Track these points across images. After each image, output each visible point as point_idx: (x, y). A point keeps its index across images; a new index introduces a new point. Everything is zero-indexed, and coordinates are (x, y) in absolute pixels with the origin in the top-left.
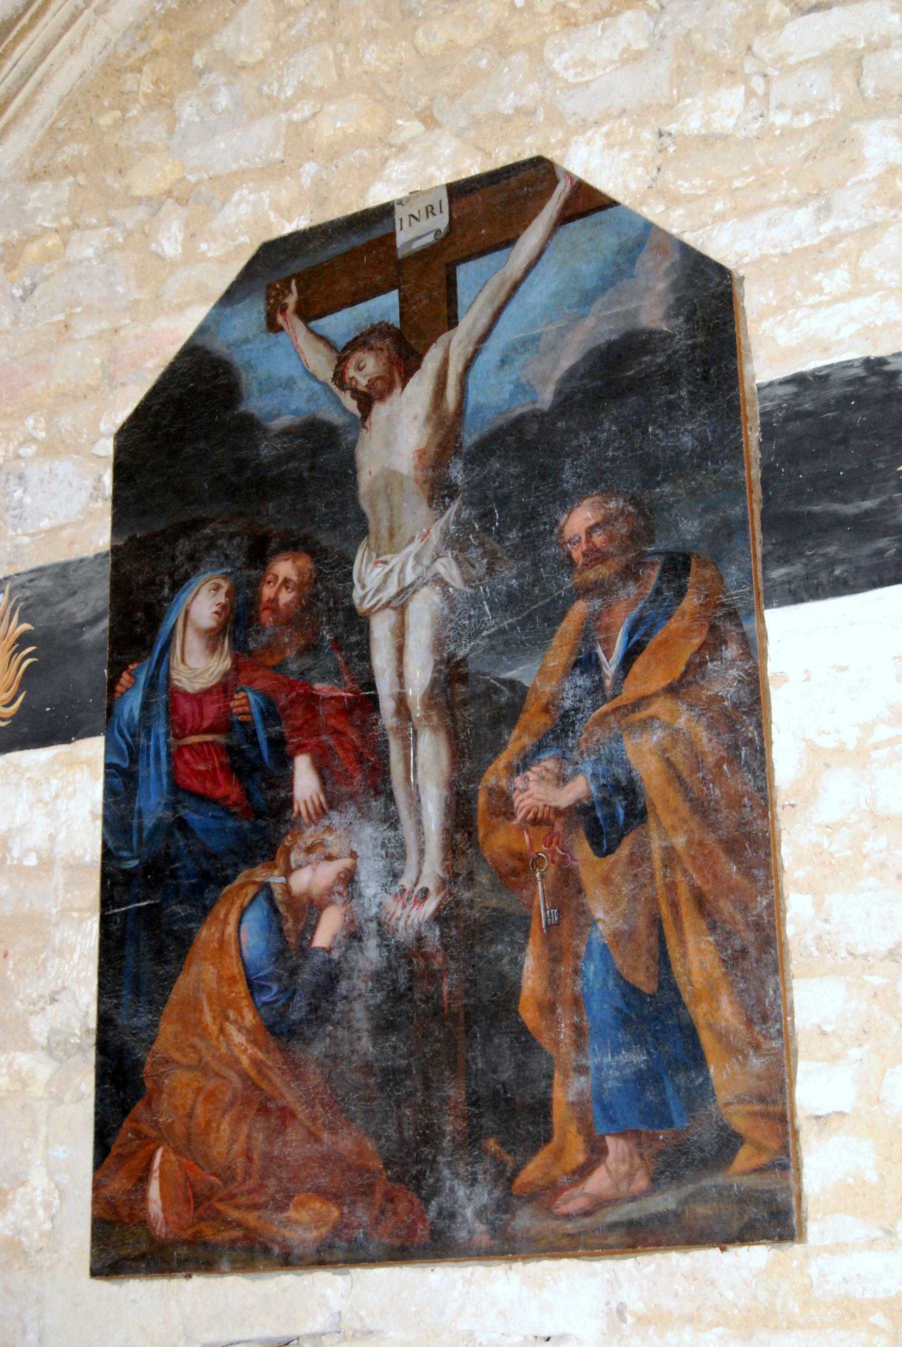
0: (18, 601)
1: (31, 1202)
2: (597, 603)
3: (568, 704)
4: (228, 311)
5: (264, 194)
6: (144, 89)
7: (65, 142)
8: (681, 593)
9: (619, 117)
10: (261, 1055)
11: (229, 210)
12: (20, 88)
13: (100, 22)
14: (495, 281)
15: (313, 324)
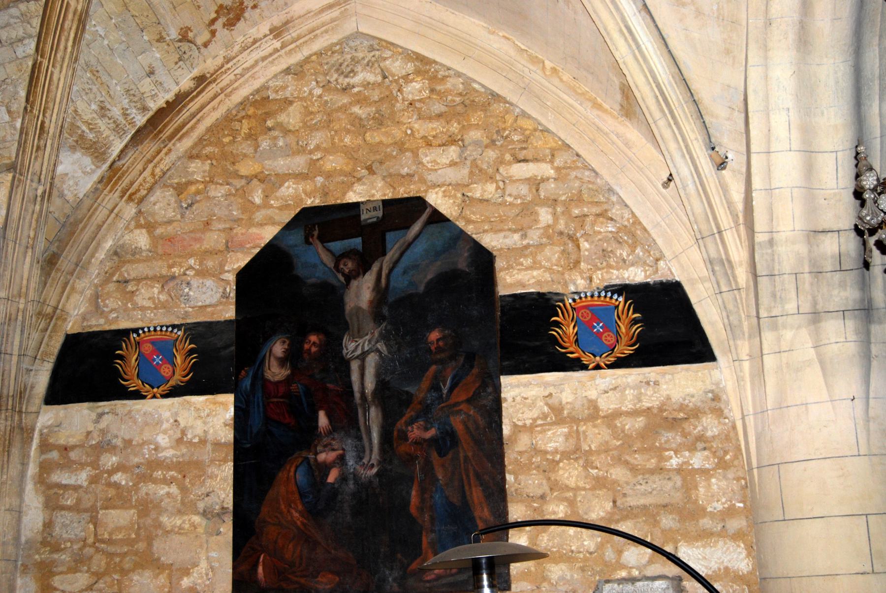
0: (188, 335)
1: (201, 573)
2: (440, 367)
3: (429, 402)
4: (287, 232)
5: (300, 186)
6: (243, 131)
7: (207, 145)
8: (472, 367)
9: (448, 185)
10: (305, 521)
11: (283, 189)
12: (190, 121)
13: (227, 100)
14: (402, 241)
15: (325, 244)
